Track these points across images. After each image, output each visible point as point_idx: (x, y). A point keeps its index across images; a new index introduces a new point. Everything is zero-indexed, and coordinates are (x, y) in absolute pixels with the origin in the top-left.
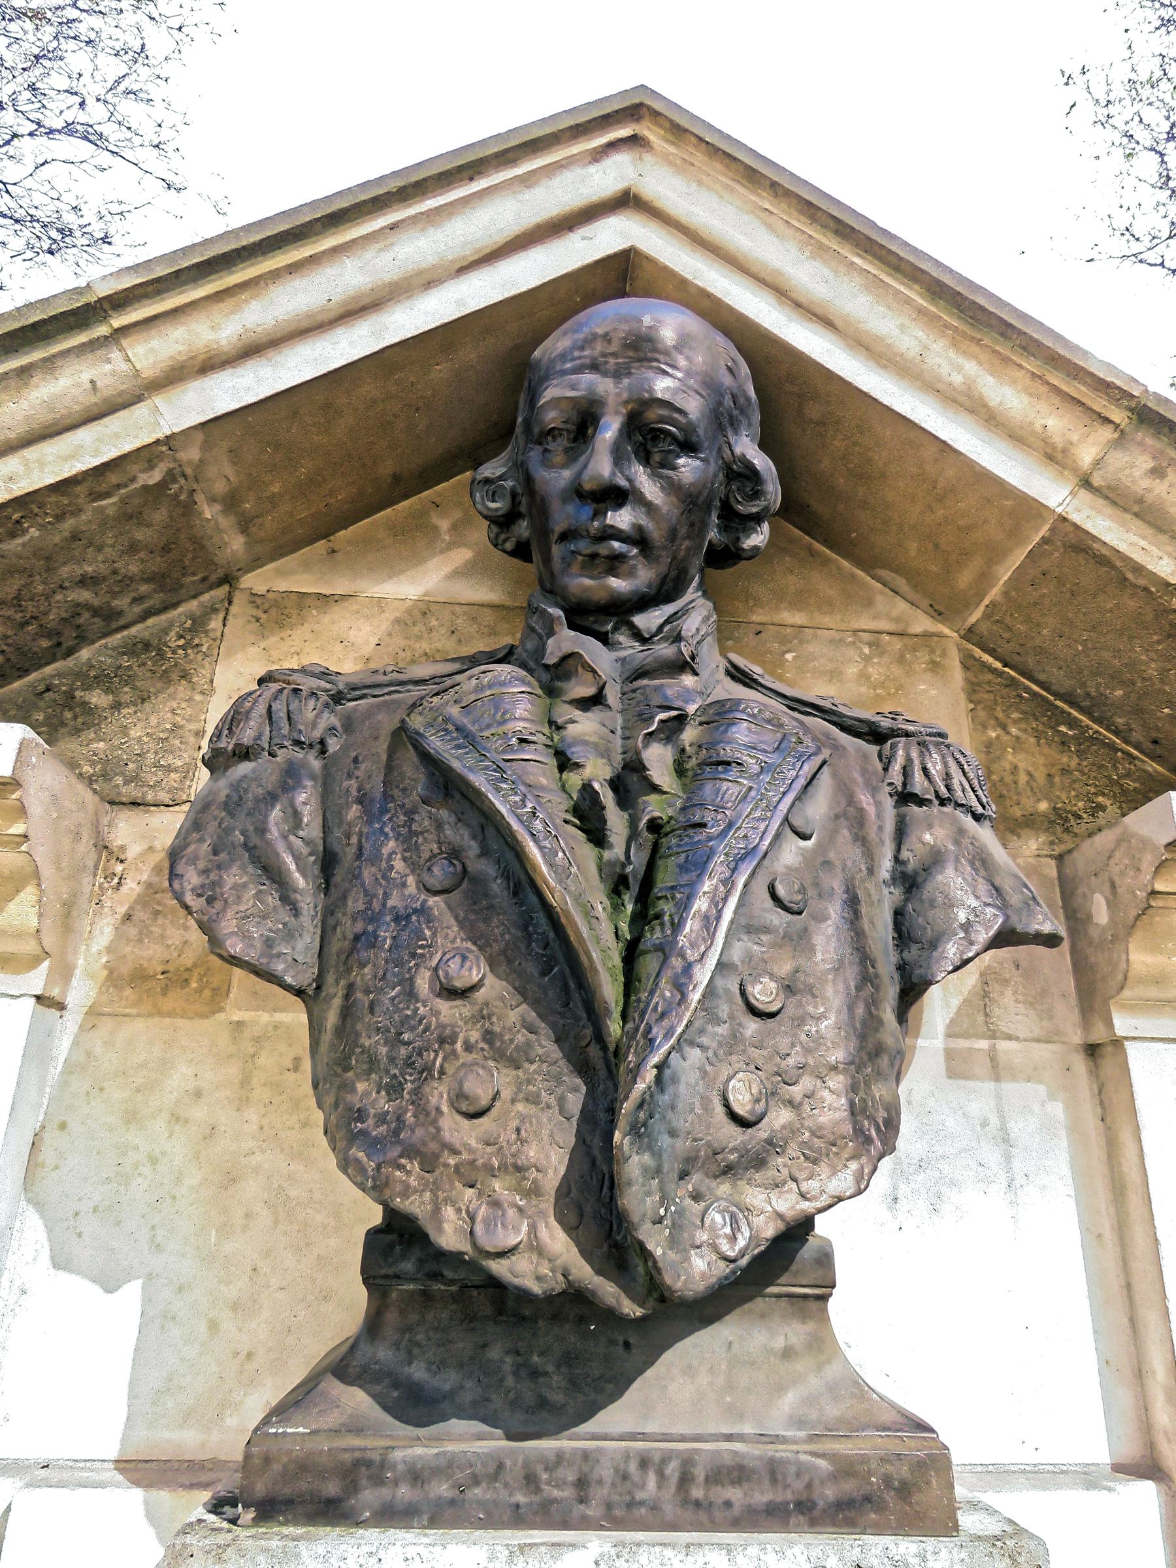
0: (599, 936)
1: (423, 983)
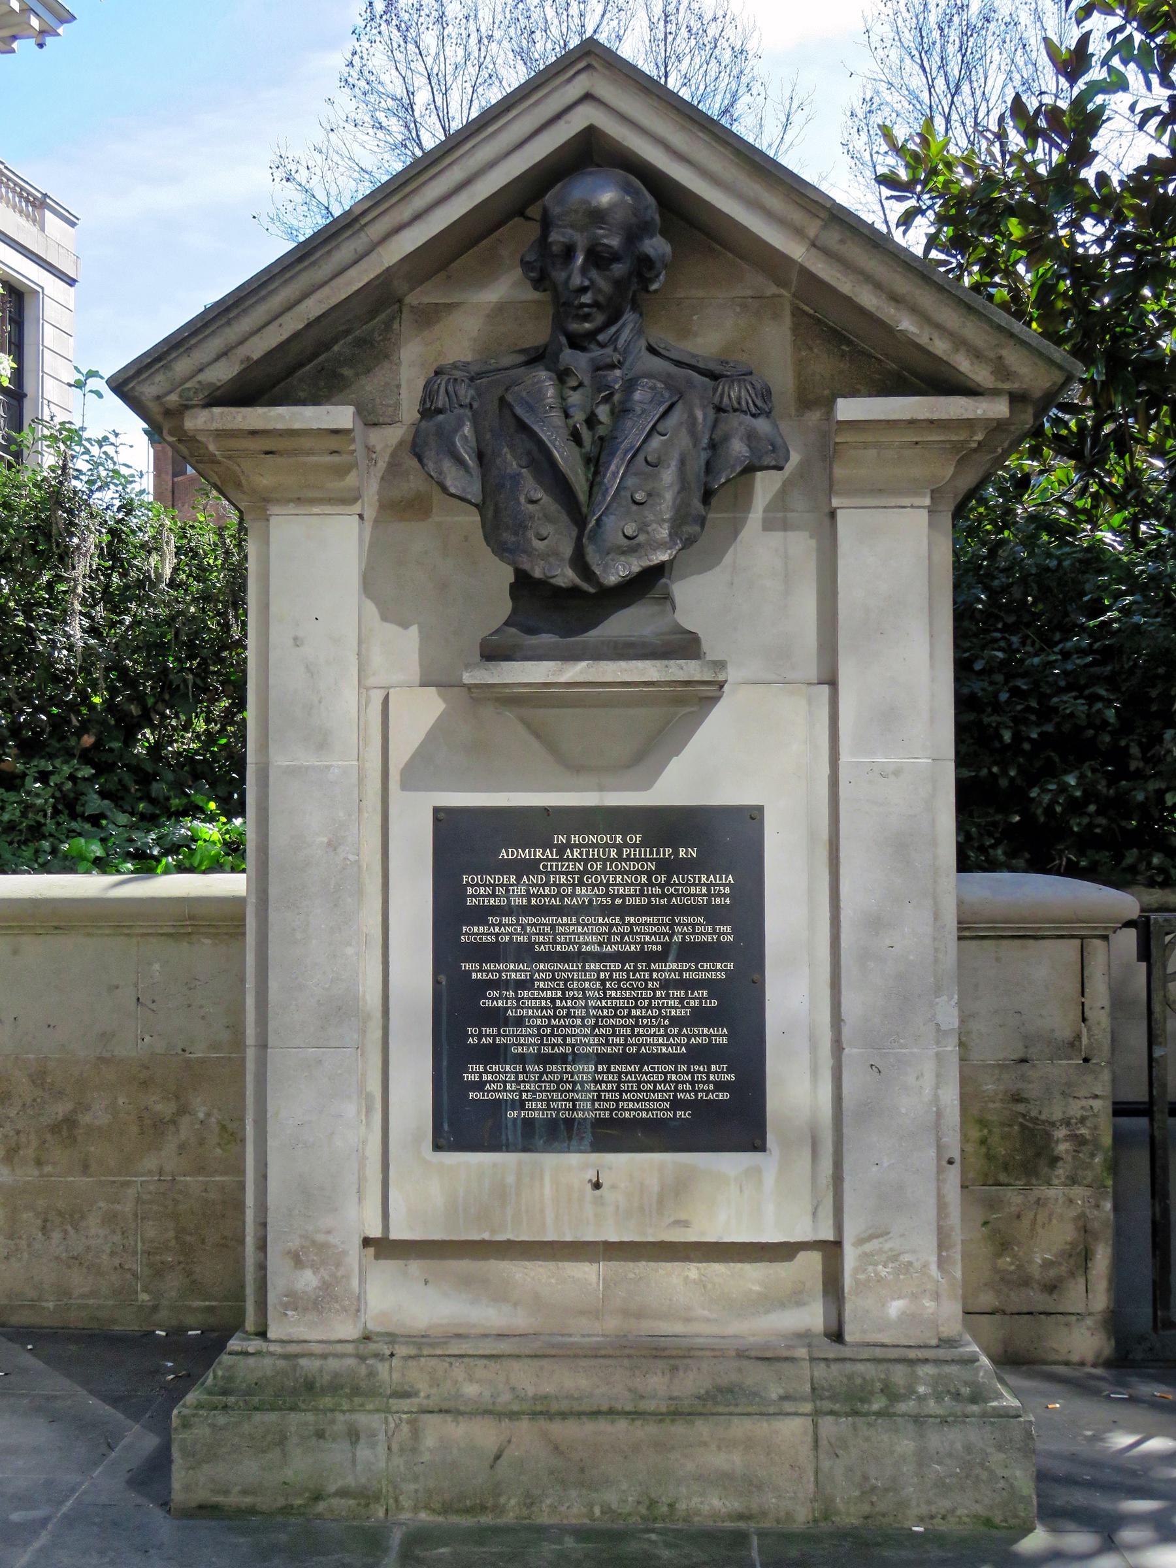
0: (578, 478)
1: (522, 500)
